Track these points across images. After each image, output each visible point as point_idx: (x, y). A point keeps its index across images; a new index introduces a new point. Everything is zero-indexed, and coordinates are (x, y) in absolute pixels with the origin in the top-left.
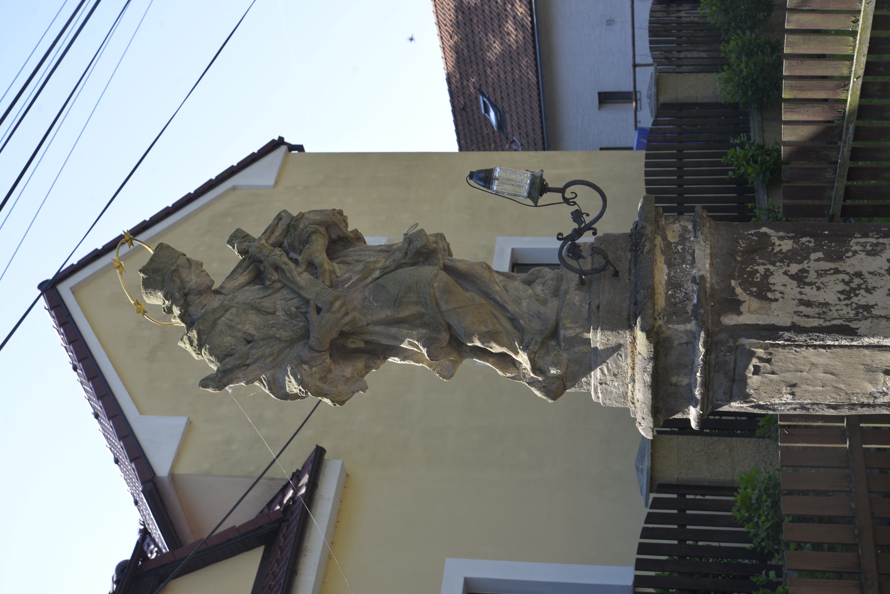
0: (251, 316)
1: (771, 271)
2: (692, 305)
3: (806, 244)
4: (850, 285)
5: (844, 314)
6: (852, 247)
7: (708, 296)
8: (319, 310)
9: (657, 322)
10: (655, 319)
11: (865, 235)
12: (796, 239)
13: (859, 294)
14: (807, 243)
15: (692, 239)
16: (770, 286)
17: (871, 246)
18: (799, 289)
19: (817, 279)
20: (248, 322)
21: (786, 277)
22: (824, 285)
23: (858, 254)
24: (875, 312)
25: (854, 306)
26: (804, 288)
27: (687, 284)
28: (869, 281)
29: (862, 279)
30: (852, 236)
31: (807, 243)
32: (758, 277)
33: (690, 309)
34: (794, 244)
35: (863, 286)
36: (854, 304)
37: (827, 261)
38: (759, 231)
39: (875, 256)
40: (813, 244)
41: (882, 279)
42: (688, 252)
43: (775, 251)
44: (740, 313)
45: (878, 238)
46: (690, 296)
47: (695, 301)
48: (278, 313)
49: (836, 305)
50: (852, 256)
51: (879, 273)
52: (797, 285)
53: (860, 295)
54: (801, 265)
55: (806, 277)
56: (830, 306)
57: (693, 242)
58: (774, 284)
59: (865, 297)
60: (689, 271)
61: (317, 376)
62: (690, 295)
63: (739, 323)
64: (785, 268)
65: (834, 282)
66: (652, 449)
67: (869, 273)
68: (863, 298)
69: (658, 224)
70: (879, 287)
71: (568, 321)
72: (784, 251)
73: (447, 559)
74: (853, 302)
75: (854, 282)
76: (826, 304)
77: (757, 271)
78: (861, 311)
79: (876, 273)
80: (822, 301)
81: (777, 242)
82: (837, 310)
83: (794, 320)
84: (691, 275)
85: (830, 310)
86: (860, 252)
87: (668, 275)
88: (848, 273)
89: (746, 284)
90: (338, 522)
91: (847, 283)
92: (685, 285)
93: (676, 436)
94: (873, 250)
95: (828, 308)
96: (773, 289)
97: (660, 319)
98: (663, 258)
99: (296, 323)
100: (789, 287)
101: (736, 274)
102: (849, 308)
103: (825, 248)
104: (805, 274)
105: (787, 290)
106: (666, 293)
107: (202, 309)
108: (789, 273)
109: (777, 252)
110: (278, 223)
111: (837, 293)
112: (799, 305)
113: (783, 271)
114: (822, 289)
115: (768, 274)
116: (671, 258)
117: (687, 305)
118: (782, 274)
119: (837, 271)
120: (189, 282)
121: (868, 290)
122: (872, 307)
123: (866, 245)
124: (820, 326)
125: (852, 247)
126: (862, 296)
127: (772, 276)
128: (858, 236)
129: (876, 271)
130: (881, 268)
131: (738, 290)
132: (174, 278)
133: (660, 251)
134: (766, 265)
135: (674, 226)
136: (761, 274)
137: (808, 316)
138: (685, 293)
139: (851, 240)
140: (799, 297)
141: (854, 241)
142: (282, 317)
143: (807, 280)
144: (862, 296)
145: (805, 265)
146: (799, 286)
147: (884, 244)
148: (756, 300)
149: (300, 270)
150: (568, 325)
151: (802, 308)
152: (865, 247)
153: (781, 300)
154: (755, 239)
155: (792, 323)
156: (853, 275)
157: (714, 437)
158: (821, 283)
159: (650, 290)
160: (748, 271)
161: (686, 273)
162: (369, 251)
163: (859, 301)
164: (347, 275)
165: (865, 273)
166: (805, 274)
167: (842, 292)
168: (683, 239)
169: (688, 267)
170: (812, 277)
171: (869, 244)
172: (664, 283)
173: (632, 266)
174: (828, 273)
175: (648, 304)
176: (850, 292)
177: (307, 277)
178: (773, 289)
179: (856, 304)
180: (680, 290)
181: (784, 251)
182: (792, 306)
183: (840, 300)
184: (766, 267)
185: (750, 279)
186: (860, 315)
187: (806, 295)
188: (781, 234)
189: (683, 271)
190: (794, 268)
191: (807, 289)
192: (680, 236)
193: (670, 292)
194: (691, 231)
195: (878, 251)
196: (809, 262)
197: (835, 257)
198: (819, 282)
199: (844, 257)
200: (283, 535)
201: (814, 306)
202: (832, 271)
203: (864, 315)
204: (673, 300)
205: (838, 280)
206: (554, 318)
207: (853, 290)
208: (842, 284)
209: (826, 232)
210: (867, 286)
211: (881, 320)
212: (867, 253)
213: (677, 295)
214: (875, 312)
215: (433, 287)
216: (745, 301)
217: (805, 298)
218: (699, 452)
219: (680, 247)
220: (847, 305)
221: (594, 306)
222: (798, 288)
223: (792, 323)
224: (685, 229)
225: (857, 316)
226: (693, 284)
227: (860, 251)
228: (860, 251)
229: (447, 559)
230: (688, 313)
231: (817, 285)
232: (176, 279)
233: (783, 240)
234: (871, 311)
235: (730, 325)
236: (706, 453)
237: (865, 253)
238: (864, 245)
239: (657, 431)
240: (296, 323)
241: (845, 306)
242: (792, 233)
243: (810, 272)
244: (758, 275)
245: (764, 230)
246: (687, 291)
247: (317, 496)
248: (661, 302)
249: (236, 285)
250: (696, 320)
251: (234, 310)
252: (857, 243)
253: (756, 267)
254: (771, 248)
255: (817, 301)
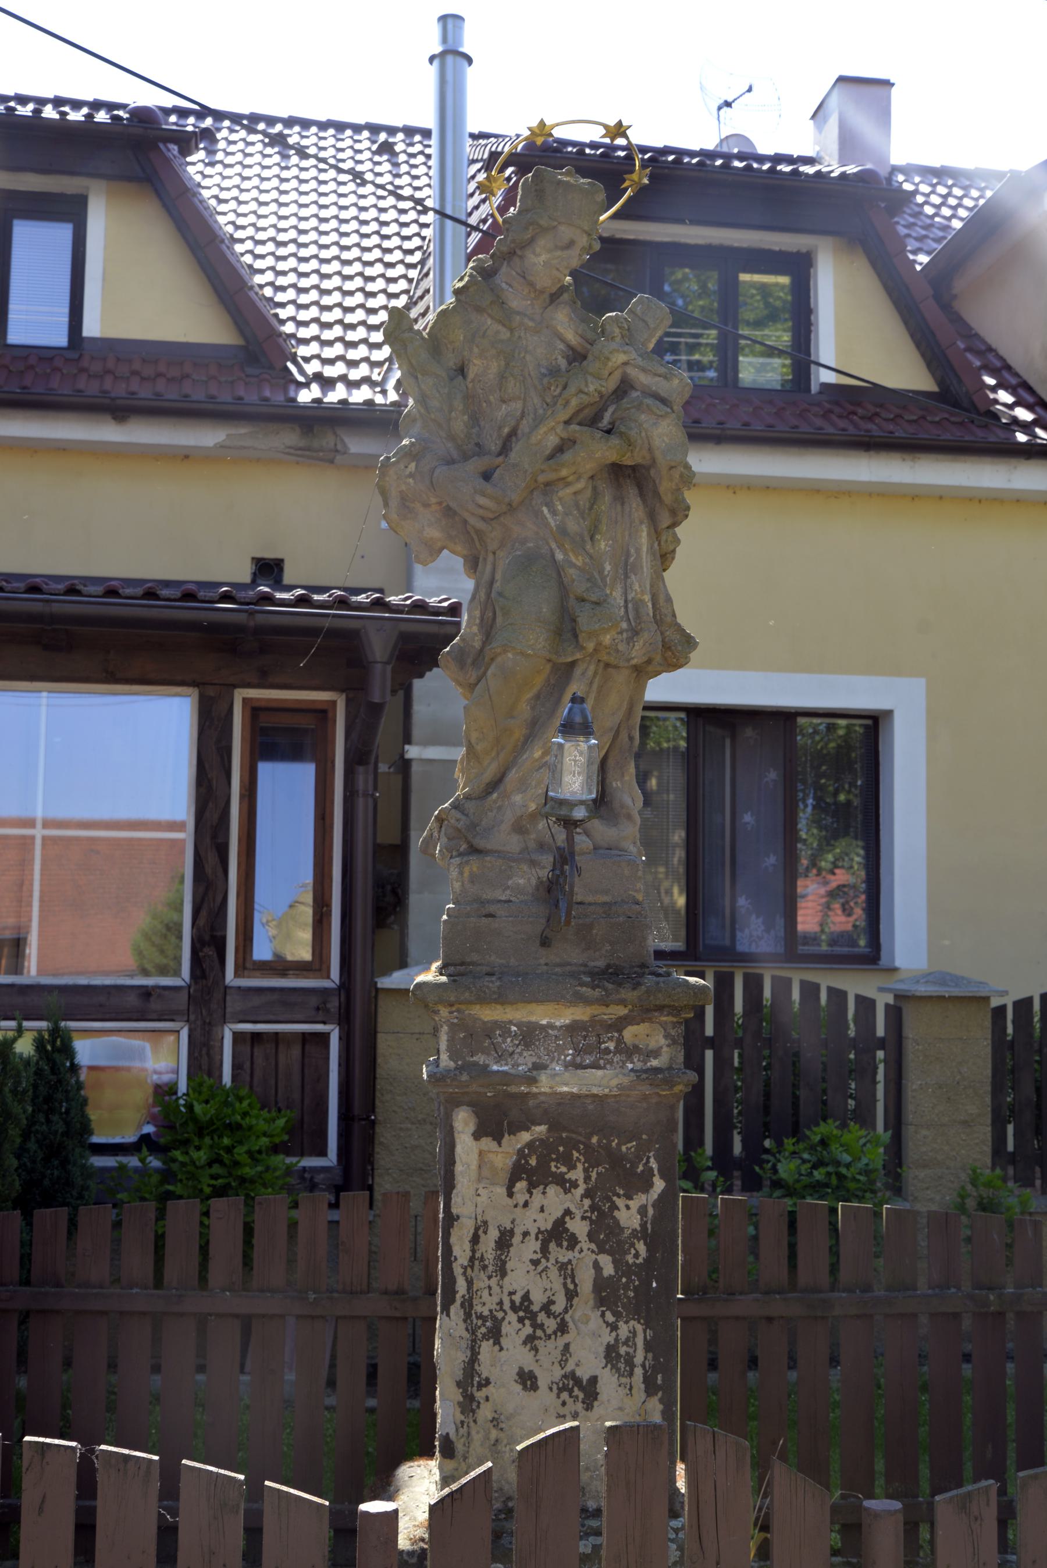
0: (495, 364)
1: (573, 1190)
2: (487, 1062)
3: (632, 1249)
4: (543, 1312)
5: (481, 1297)
6: (626, 1322)
7: (500, 1087)
8: (487, 476)
9: (445, 1007)
10: (451, 1005)
11: (648, 1347)
12: (642, 1234)
13: (524, 1325)
14: (633, 1251)
15: (630, 1066)
16: (542, 1187)
17: (627, 1354)
18: (533, 1232)
19: (554, 1262)
20: (485, 362)
21: (559, 1214)
22: (542, 1271)
23: (611, 1331)
24: (486, 1348)
25: (500, 1315)
26: (537, 1239)
27: (531, 1055)
28: (551, 1344)
29: (555, 1333)
30: (647, 1325)
31: (633, 1251)
32: (558, 1168)
33: (480, 1059)
34: (630, 1231)
35: (539, 1333)
36: (503, 1314)
37: (594, 1281)
38: (654, 1175)
39: (605, 1358)
40: (631, 1261)
41: (553, 1363)
42: (600, 1058)
43: (615, 1198)
44: (477, 1136)
45: (643, 1366)
46: (506, 1060)
47: (495, 1068)
48: (504, 406)
49: (501, 1287)
50: (607, 1324)
51: (567, 1360)
52: (543, 1229)
53: (520, 1326)
54: (587, 1239)
55: (560, 1245)
56: (499, 1277)
57: (622, 1067)
58: (544, 1193)
59: (517, 1333)
60: (559, 1059)
61: (403, 488)
62: (509, 1060)
63: (456, 1135)
64: (578, 1214)
65: (549, 1288)
66: (950, 997)
67: (567, 1346)
68: (513, 1330)
69: (655, 1011)
70: (537, 1358)
71: (475, 869)
72: (616, 1213)
73: (922, 681)
74: (506, 1314)
75: (548, 1320)
76: (502, 1272)
77: (572, 1167)
78: (488, 1324)
79: (568, 1355)
80: (509, 1266)
81: (634, 1204)
82: (490, 1288)
83: (462, 1220)
84: (551, 1062)
85: (490, 1277)
86: (614, 1334)
87: (551, 1026)
88: (566, 1311)
89: (541, 1148)
90: (980, 501)
91: (546, 1307)
92: (530, 1053)
93: (990, 1036)
94: (619, 1356)
95: (494, 1274)
96: (534, 1191)
97: (451, 1013)
98: (585, 1018)
99: (494, 438)
100: (540, 1217)
101: (564, 1135)
102: (494, 1307)
103: (624, 1280)
104: (565, 1244)
105: (532, 1212)
106: (511, 1022)
107: (507, 283)
108: (567, 1219)
109: (613, 1203)
110: (660, 376)
111: (526, 1290)
112: (499, 1230)
113: (573, 1209)
114: (534, 1267)
115: (567, 1186)
116: (587, 1031)
117: (488, 1054)
118: (566, 1206)
119: (571, 1295)
120: (534, 253)
121: (530, 1340)
122: (497, 1342)
123: (628, 1346)
124: (453, 1259)
125: (626, 1322)
126: (520, 1329)
127: (562, 1190)
128: (648, 1334)
129: (571, 1356)
130: (577, 1365)
131: (525, 1137)
132: (531, 228)
133: (596, 1013)
134: (585, 1182)
135: (661, 1036)
136: (566, 1173)
137: (475, 1240)
138: (513, 1053)
139: (639, 1322)
140: (518, 1231)
141: (639, 1328)
142: (500, 414)
143: (552, 1246)
144: (520, 1329)
145: (585, 1244)
146: (539, 1232)
147: (631, 1374)
148: (510, 1163)
149: (560, 429)
150: (467, 870)
151: (493, 1234)
152: (626, 1343)
153: (510, 1202)
154: (638, 1167)
155: (458, 1217)
156: (563, 1319)
157: (990, 1096)
158: (547, 1267)
159: (495, 996)
160: (573, 1155)
161: (556, 1054)
162: (630, 535)
163: (510, 1323)
164: (560, 508)
165: (567, 1338)
166: (565, 1244)
167: (526, 1297)
168: (628, 1052)
169: (569, 1058)
170: (559, 1253)
171: (631, 1351)
172: (533, 1019)
173: (568, 968)
174: (569, 1281)
175: (467, 994)
176: (527, 1310)
177: (549, 444)
178: (534, 1191)
179: (503, 1319)
180: (518, 1046)
181: (616, 1213)
182: (499, 1219)
183: (511, 1294)
184: (581, 1182)
185: (554, 1156)
186: (480, 1322)
187: (522, 1242)
188: (651, 1211)
189: (561, 1050)
190: (579, 1227)
191: (533, 1245)
192: (636, 1047)
193: (514, 1028)
194: (646, 1064)
195: (617, 1364)
196: (593, 1252)
197: (604, 1294)
198: (549, 1265)
199: (604, 1309)
200: (946, 419)
201: (498, 1252)
202: (571, 1287)
203: (479, 1328)
204: (498, 1032)
205: (553, 1295)
206: (489, 847)
207: (533, 1317)
208: (545, 1300)
209: (654, 1285)
210: (541, 1338)
211: (465, 1352)
212: (613, 1346)
213: (509, 1040)
214: (486, 1348)
215: (505, 652)
216: (500, 1146)
217: (517, 1239)
218: (960, 1073)
219: (611, 1045)
220: (501, 1303)
221: (492, 909)
222: (537, 1230)
223: (458, 1217)
224: (656, 1053)
225: (478, 1318)
226: (530, 1065)
227: (618, 1335)
228: (618, 1335)
229: (922, 681)
230: (472, 1056)
231: (543, 1260)
232: (530, 231)
233: (639, 1212)
234: (488, 1340)
235: (452, 1120)
236: (958, 1083)
237: (613, 1342)
238: (630, 1343)
239: (1001, 1010)
240: (494, 438)
241: (498, 1300)
242: (652, 1228)
243: (570, 1252)
244: (564, 1169)
245: (659, 1185)
246: (516, 1056)
247: (1014, 461)
248: (489, 1014)
249: (559, 328)
250: (456, 1069)
251: (505, 334)
252: (634, 1333)
253: (580, 1167)
254: (622, 1192)
255: (508, 1258)
